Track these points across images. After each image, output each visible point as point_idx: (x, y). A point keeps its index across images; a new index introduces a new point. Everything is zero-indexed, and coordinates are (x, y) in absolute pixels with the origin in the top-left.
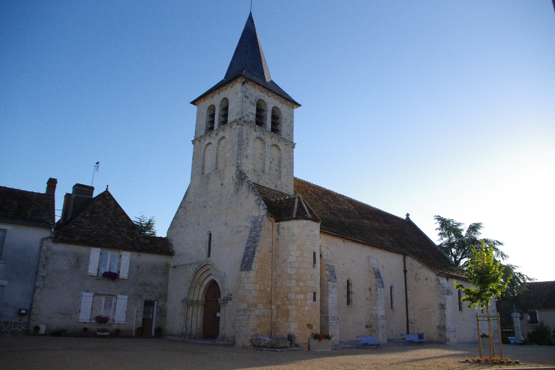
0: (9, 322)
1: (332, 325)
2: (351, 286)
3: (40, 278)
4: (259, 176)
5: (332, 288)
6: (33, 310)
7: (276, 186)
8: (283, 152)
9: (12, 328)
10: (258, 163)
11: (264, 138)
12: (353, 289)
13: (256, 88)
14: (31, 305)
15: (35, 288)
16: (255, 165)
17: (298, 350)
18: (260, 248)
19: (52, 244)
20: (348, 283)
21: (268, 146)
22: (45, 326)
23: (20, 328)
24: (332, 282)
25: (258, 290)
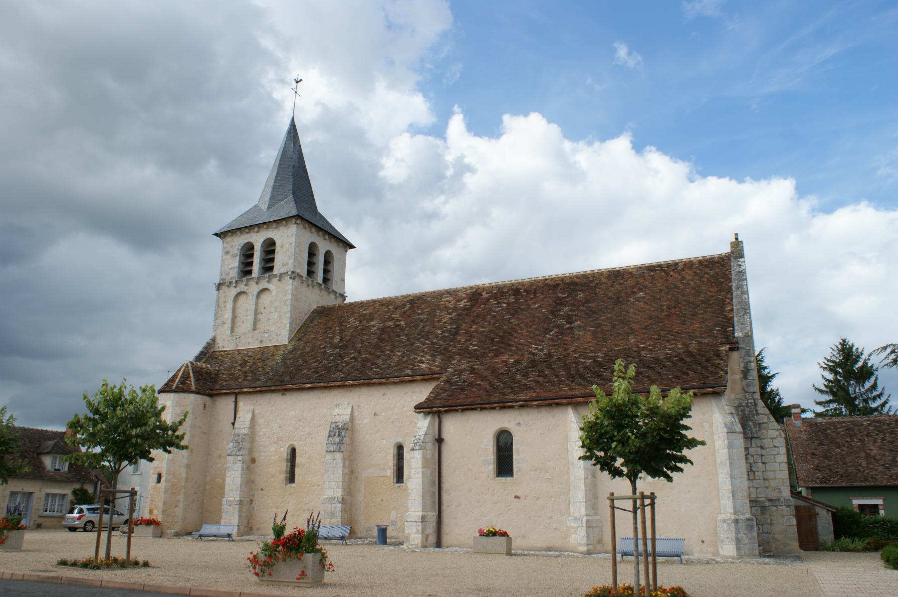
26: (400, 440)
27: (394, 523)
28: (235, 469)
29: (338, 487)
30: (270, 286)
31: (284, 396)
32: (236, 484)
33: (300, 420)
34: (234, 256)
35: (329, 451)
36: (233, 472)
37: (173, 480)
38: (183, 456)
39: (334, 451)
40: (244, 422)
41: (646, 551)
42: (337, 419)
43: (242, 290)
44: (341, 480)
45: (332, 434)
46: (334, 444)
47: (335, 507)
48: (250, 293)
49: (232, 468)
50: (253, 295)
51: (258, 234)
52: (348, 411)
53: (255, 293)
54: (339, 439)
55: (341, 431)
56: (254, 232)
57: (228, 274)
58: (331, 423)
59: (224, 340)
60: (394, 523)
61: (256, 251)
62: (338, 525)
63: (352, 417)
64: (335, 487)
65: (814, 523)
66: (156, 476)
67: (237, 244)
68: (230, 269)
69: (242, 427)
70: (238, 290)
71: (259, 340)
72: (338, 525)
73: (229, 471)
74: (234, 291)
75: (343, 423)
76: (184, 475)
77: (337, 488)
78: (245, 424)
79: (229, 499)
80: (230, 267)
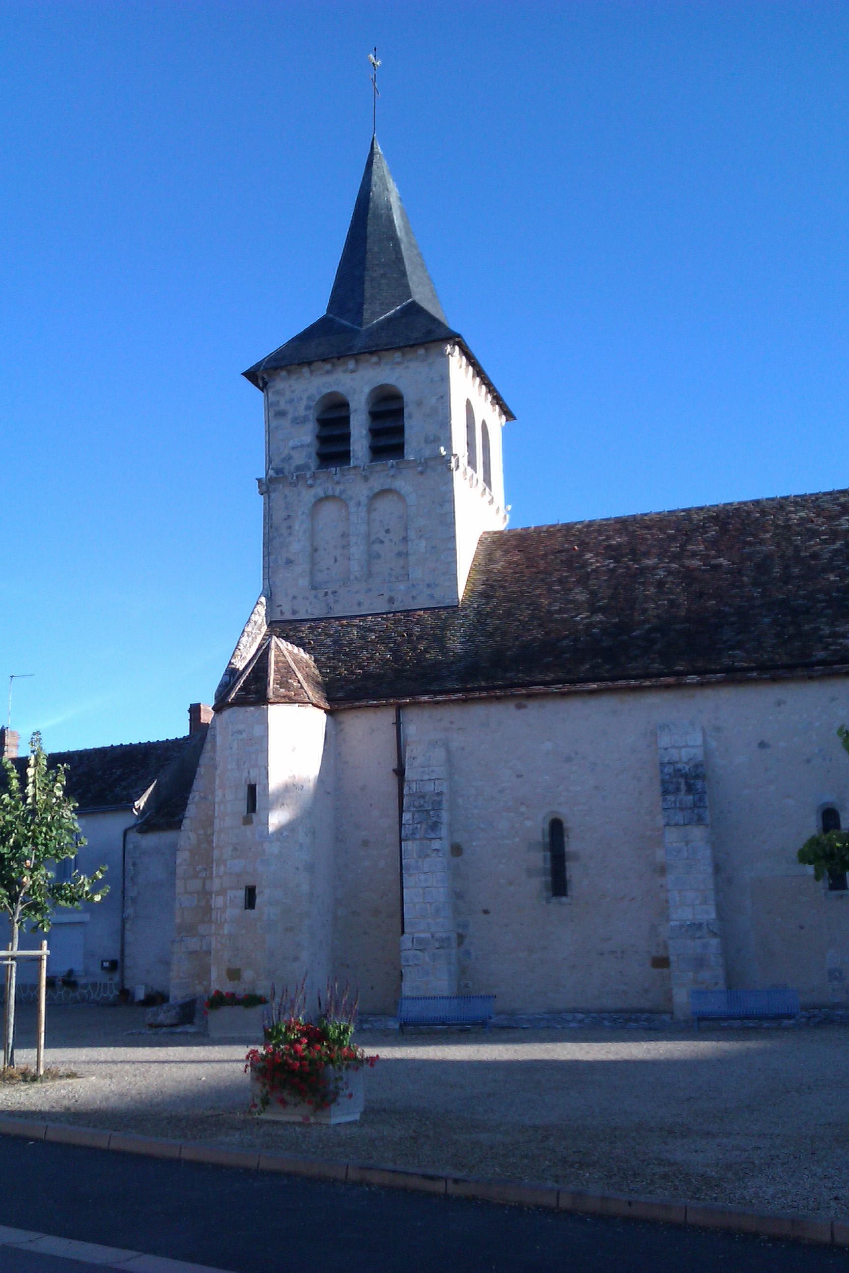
0: (96, 984)
1: (416, 965)
2: (568, 836)
3: (130, 901)
4: (330, 596)
5: (420, 857)
6: (127, 959)
7: (391, 600)
8: (412, 499)
9: (102, 994)
10: (336, 560)
11: (343, 492)
12: (572, 845)
13: (307, 375)
14: (122, 951)
15: (124, 921)
16: (328, 569)
17: (187, 1033)
18: (202, 794)
19: (138, 836)
20: (557, 828)
21: (359, 504)
22: (143, 987)
23: (111, 992)
24: (418, 842)
25: (198, 892)
26: (829, 798)
27: (837, 974)
28: (426, 870)
29: (705, 902)
30: (399, 484)
31: (523, 711)
32: (431, 904)
33: (569, 759)
34: (298, 421)
35: (673, 822)
36: (422, 877)
37: (284, 901)
38: (301, 845)
39: (685, 825)
40: (429, 766)
41: (300, 1124)
42: (674, 754)
43: (330, 493)
44: (711, 887)
45: (671, 788)
46: (681, 809)
47: (705, 946)
48: (351, 498)
49: (417, 868)
50: (359, 504)
51: (354, 375)
52: (699, 741)
53: (364, 500)
54: (691, 798)
55: (692, 782)
56: (345, 371)
57: (289, 458)
58: (662, 764)
59: (294, 598)
60: (837, 974)
61: (356, 411)
62: (716, 984)
63: (707, 753)
64: (697, 902)
65: (838, 1018)
66: (242, 894)
67: (305, 397)
68: (293, 448)
69: (426, 777)
70: (319, 491)
71: (386, 597)
72: (716, 984)
73: (410, 875)
74: (308, 496)
75: (691, 764)
76: (305, 888)
77: (701, 904)
78: (433, 771)
79: (415, 935)
80: (291, 443)
